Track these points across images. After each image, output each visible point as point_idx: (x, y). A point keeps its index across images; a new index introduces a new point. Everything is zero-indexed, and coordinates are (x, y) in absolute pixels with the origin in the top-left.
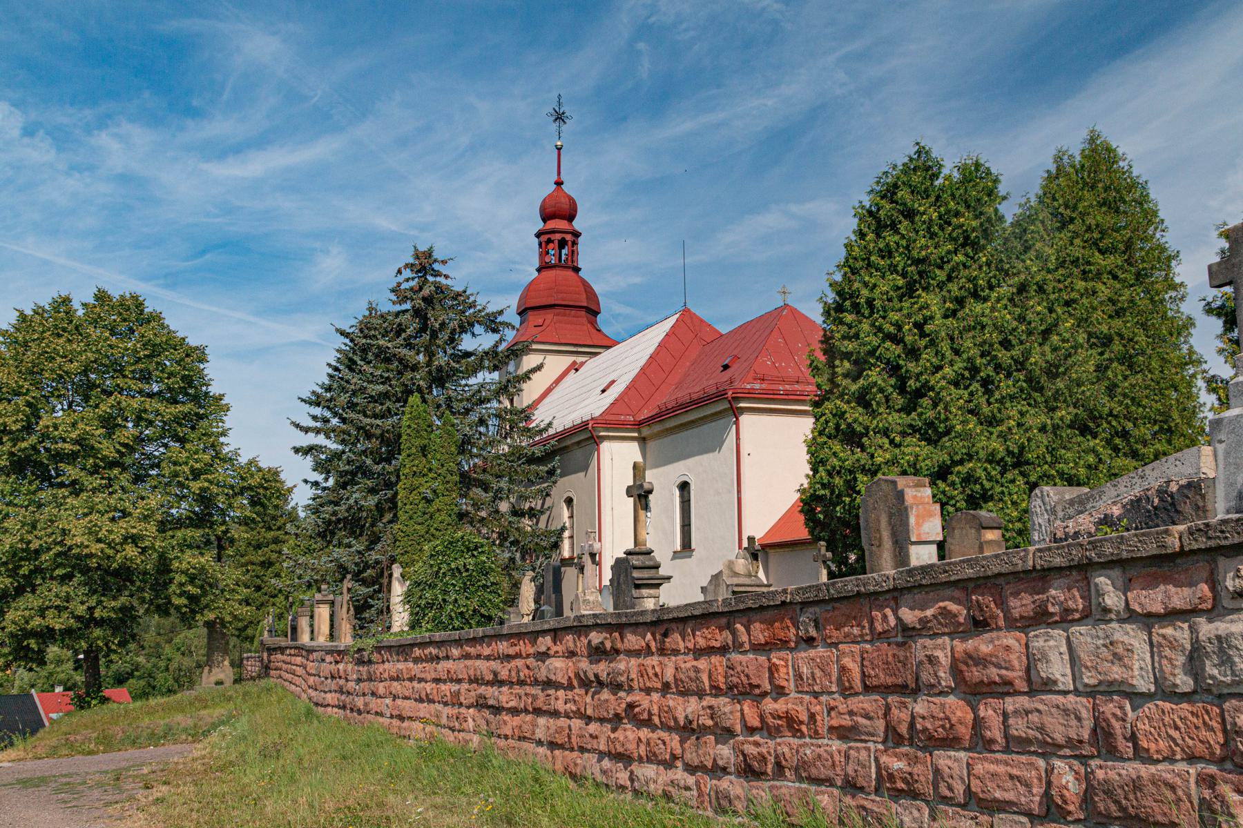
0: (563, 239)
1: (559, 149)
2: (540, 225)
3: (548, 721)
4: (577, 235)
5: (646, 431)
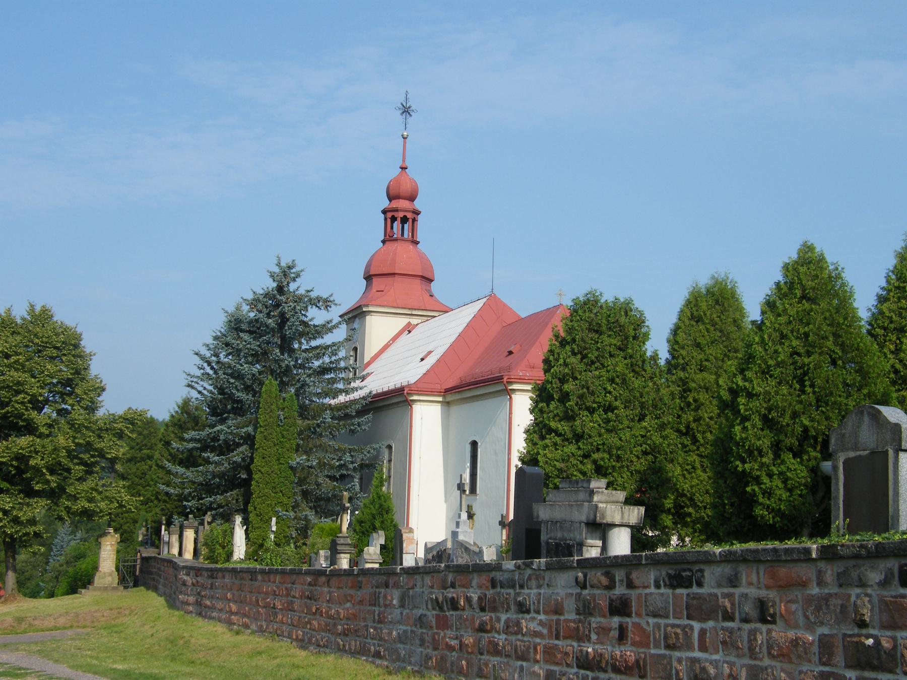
0: (405, 216)
1: (405, 138)
2: (385, 203)
3: (111, 574)
4: (417, 213)
5: (449, 398)
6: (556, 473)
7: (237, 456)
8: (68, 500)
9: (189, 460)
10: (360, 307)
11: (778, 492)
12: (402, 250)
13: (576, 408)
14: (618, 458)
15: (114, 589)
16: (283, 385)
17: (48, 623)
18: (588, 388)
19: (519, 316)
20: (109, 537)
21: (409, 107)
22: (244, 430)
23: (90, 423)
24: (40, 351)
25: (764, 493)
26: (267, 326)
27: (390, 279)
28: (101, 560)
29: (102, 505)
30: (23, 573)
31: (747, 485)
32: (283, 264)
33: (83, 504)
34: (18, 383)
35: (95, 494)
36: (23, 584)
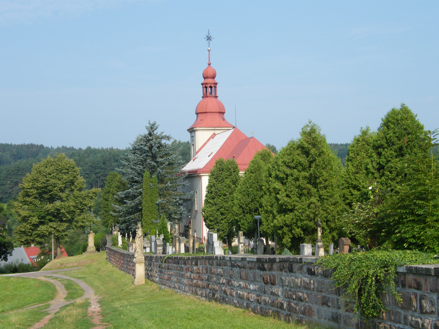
1: (209, 51)
2: (202, 80)
3: (93, 247)
4: (216, 84)
6: (210, 215)
7: (137, 201)
8: (75, 222)
9: (121, 201)
10: (192, 128)
11: (245, 224)
12: (210, 101)
13: (215, 196)
14: (228, 210)
15: (94, 252)
16: (151, 174)
17: (71, 265)
18: (218, 189)
19: (246, 137)
20: (91, 234)
21: (210, 37)
22: (139, 190)
23: (80, 195)
24: (61, 171)
25: (242, 225)
26: (145, 150)
27: (205, 114)
28: (89, 242)
29: (87, 223)
30: (73, 238)
31: (238, 222)
32: (151, 123)
33: (80, 224)
34: (55, 184)
35: (84, 220)
36: (73, 244)
